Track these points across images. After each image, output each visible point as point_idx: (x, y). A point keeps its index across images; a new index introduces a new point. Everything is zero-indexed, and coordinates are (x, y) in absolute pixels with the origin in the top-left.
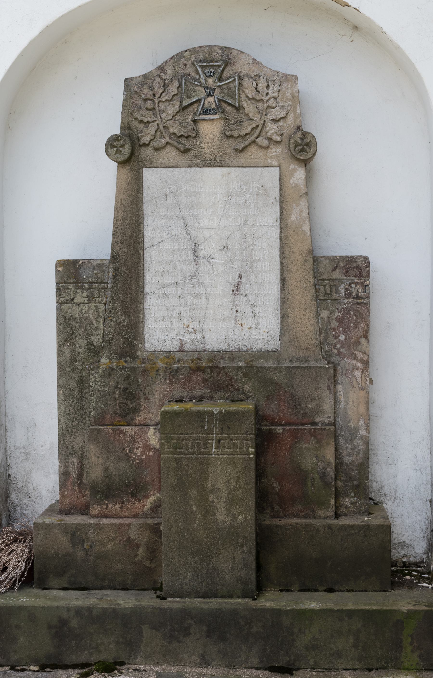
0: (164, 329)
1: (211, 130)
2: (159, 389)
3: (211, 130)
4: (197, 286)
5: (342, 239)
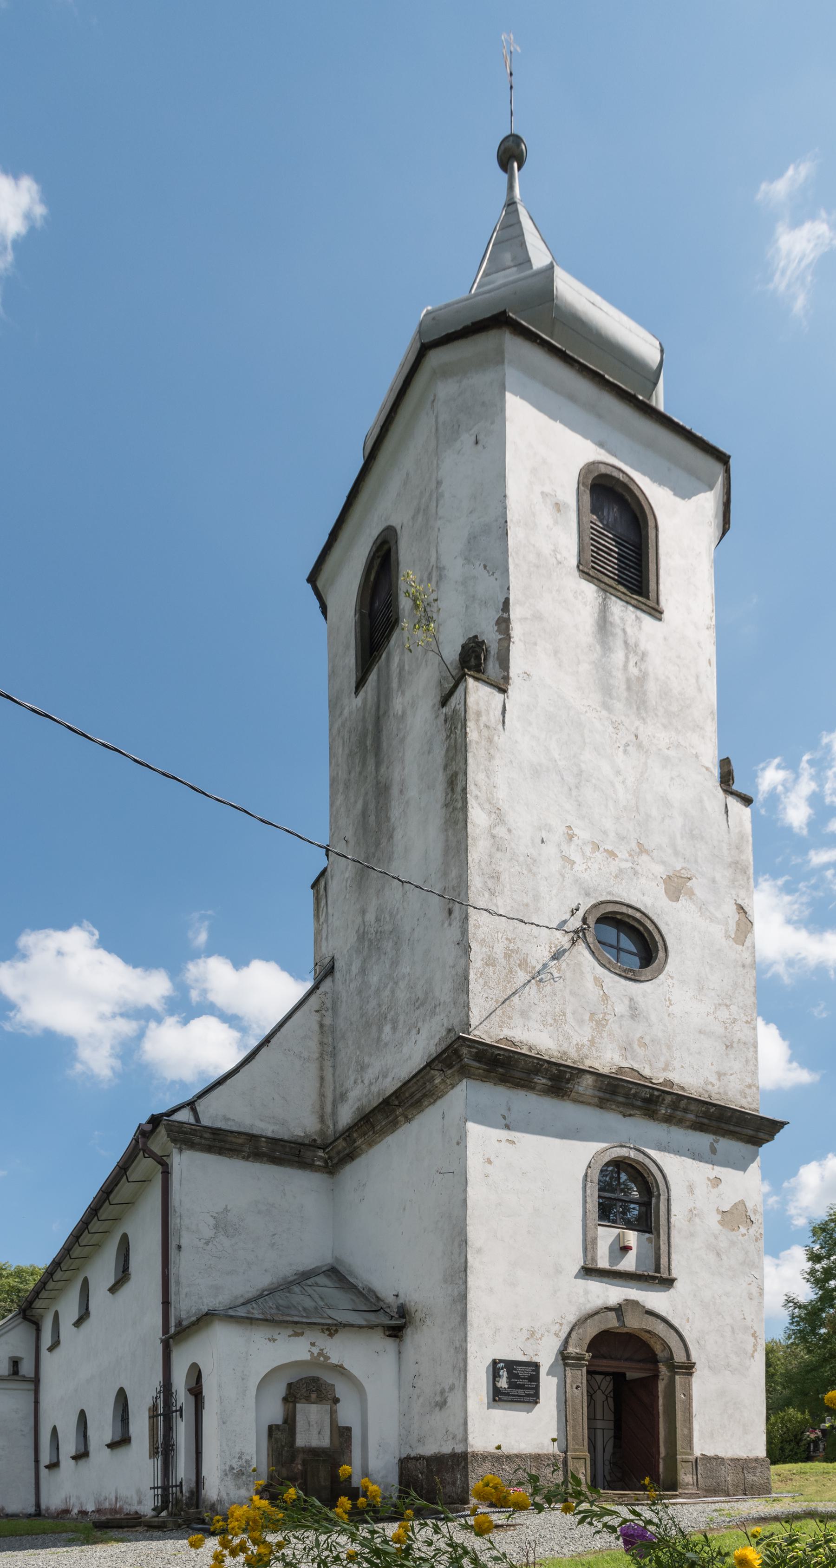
0: (301, 1441)
1: (314, 1396)
3: (314, 1396)
5: (343, 1422)
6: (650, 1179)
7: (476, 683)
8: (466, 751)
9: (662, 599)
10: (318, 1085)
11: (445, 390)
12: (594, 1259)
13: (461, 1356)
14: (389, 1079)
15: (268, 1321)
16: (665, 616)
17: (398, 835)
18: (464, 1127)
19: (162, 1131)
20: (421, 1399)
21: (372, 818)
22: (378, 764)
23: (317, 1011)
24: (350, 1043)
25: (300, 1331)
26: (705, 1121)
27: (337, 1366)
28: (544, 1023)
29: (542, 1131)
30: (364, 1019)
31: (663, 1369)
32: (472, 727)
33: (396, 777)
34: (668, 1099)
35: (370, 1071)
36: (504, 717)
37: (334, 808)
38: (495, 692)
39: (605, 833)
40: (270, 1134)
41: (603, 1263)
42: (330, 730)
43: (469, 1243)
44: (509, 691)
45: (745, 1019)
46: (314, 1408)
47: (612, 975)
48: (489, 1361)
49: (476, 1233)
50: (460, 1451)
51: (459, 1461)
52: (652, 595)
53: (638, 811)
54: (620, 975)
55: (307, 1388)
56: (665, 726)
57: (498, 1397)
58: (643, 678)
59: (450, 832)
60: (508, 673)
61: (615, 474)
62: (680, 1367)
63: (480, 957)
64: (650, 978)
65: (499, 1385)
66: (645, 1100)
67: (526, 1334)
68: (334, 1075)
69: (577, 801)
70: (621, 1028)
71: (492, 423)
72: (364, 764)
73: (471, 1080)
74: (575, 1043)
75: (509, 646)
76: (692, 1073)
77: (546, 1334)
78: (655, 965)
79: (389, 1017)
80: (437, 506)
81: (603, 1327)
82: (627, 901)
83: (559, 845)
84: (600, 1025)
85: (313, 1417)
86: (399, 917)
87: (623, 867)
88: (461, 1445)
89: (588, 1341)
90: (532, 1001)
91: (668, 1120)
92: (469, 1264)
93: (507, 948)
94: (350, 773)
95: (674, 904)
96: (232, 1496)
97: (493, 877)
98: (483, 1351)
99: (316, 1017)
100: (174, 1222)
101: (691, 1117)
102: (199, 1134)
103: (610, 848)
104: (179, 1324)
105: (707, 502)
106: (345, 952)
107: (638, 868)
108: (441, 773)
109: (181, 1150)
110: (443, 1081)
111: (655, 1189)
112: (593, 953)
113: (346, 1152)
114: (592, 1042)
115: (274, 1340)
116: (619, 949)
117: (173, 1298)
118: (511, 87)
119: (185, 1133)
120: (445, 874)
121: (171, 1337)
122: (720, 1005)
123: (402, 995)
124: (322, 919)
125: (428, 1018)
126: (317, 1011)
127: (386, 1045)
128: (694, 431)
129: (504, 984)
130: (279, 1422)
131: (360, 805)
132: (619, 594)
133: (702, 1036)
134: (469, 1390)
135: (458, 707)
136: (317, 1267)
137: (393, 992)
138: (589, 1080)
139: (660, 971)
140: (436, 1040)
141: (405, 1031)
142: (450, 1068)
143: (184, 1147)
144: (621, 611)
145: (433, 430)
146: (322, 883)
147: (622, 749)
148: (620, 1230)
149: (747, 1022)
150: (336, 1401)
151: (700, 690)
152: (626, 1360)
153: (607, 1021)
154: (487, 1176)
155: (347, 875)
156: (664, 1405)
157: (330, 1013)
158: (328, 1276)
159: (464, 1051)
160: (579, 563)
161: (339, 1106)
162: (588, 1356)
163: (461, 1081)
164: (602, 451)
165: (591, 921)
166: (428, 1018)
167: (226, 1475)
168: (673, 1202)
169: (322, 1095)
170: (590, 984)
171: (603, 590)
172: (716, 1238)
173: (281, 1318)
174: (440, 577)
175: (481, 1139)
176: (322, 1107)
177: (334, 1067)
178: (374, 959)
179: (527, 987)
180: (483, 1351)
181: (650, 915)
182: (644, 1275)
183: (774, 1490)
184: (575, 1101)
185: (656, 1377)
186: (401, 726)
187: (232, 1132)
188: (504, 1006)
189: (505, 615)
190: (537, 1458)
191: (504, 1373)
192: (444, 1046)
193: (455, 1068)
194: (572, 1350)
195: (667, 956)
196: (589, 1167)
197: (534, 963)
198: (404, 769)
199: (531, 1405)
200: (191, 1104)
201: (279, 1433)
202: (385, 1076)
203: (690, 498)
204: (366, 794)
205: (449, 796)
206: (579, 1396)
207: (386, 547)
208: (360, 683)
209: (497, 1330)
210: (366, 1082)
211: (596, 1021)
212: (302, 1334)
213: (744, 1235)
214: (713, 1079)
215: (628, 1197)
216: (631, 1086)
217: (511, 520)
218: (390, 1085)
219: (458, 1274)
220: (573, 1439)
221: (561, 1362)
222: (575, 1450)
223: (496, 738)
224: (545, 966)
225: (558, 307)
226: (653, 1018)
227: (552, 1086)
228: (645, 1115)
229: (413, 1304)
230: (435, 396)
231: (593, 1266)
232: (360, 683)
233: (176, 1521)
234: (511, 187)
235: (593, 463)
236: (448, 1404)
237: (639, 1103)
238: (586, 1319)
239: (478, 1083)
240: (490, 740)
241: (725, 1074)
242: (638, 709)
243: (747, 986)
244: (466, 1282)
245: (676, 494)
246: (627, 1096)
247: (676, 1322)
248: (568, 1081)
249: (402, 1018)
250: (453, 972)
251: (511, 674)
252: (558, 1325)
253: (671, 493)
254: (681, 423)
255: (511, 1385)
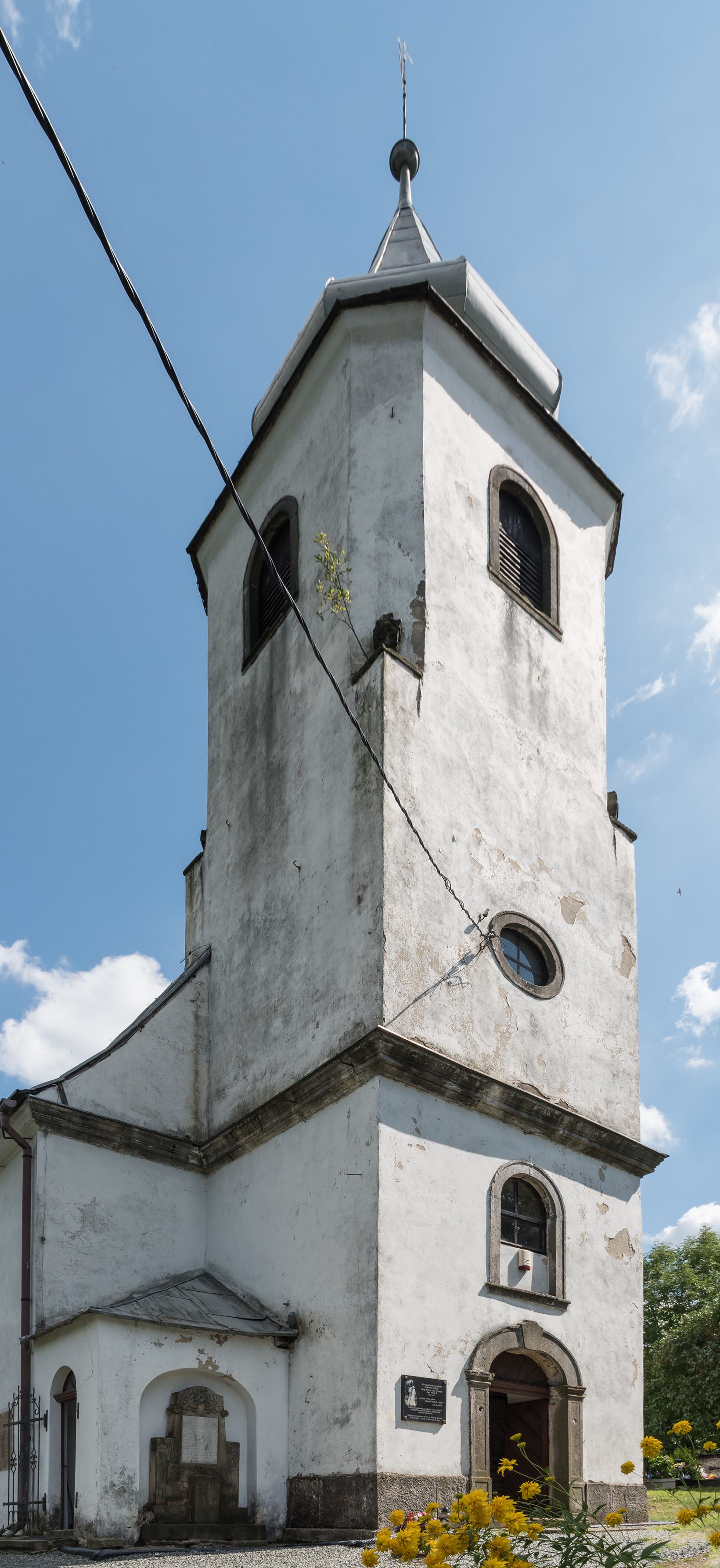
0: (187, 1457)
1: (201, 1407)
2: (187, 1473)
3: (201, 1407)
4: (566, 1536)
5: (231, 1437)
6: (546, 1200)
7: (393, 662)
8: (383, 730)
9: (562, 620)
10: (192, 1079)
11: (359, 355)
12: (497, 1277)
13: (369, 1371)
14: (278, 1076)
15: (156, 1324)
16: (565, 637)
17: (294, 819)
18: (376, 1127)
19: (26, 1109)
20: (317, 1416)
21: (261, 802)
22: (270, 745)
23: (192, 1001)
24: (230, 1037)
25: (187, 1336)
26: (597, 1146)
27: (226, 1376)
28: (453, 1027)
29: (449, 1141)
30: (248, 1012)
31: (554, 1393)
32: (389, 707)
33: (293, 757)
34: (567, 1119)
35: (255, 1066)
36: (419, 703)
37: (213, 791)
38: (410, 675)
39: (509, 842)
40: (141, 1125)
41: (504, 1282)
42: (209, 709)
43: (380, 1250)
44: (424, 677)
45: (628, 1050)
46: (201, 1421)
47: (515, 988)
48: (397, 1378)
49: (387, 1240)
50: (366, 1472)
51: (368, 1483)
52: (553, 613)
53: (539, 827)
54: (522, 989)
55: (191, 1399)
56: (563, 747)
57: (406, 1415)
58: (544, 694)
59: (361, 816)
60: (423, 658)
61: (522, 483)
62: (573, 1392)
63: (394, 949)
64: (548, 996)
65: (408, 1403)
66: (546, 1119)
67: (433, 1351)
68: (209, 1070)
69: (485, 805)
70: (522, 1043)
71: (409, 398)
72: (252, 743)
73: (384, 1078)
74: (481, 1052)
75: (424, 631)
76: (584, 1096)
77: (452, 1351)
78: (553, 984)
79: (280, 1010)
80: (349, 475)
81: (505, 1347)
82: (530, 916)
83: (468, 847)
84: (504, 1037)
85: (200, 1431)
86: (294, 904)
87: (525, 880)
88: (369, 1466)
89: (491, 1360)
90: (442, 1003)
91: (564, 1141)
92: (380, 1273)
93: (420, 944)
94: (234, 754)
95: (570, 926)
96: (113, 1515)
97: (407, 867)
98: (394, 1364)
99: (191, 1007)
100: (37, 1211)
101: (585, 1140)
102: (67, 1117)
103: (514, 859)
104: (41, 1324)
105: (600, 534)
106: (225, 941)
107: (538, 883)
108: (350, 754)
109: (46, 1133)
110: (352, 1077)
111: (551, 1211)
112: (498, 962)
113: (226, 1151)
114: (497, 1053)
115: (161, 1345)
116: (519, 964)
117: (34, 1295)
118: (404, 95)
119: (53, 1115)
120: (354, 860)
121: (34, 1338)
122: (608, 1033)
123: (297, 987)
124: (196, 906)
125: (329, 1011)
126: (192, 1001)
127: (276, 1039)
128: (593, 459)
129: (417, 981)
130: (163, 1435)
131: (246, 787)
132: (524, 605)
133: (593, 1062)
134: (378, 1407)
135: (372, 684)
136: (189, 1272)
137: (285, 983)
138: (496, 1091)
139: (558, 990)
140: (341, 1034)
141: (300, 1025)
142: (361, 1064)
143: (49, 1130)
144: (526, 623)
145: (345, 396)
146: (197, 869)
147: (525, 761)
148: (518, 1249)
149: (630, 1053)
150: (224, 1414)
151: (593, 719)
152: (521, 1382)
153: (510, 1034)
154: (398, 1181)
155: (229, 861)
156: (555, 1430)
157: (205, 1005)
158: (204, 1282)
159: (381, 1045)
160: (489, 564)
161: (215, 1103)
162: (491, 1376)
163: (372, 1077)
164: (510, 458)
165: (497, 930)
166: (329, 1011)
167: (107, 1492)
168: (567, 1225)
169: (196, 1090)
170: (495, 994)
171: (510, 597)
172: (603, 1264)
173: (168, 1321)
174: (351, 550)
175: (393, 1143)
176: (196, 1103)
177: (209, 1062)
178: (262, 949)
179: (438, 988)
180: (394, 1364)
181: (549, 933)
182: (542, 1297)
183: (650, 1518)
184: (481, 1112)
185: (545, 1401)
186: (300, 705)
187: (103, 1118)
188: (416, 1003)
189: (421, 599)
190: (443, 1482)
191: (413, 1391)
192: (349, 1042)
193: (365, 1065)
194: (477, 1369)
195: (563, 977)
196: (493, 1181)
197: (445, 964)
198: (303, 749)
199: (437, 1425)
200: (58, 1084)
201: (164, 1447)
202: (274, 1072)
203: (585, 528)
204: (255, 776)
205: (360, 778)
206: (482, 1418)
207: (282, 519)
208: (248, 660)
209: (406, 1345)
210: (250, 1078)
211: (501, 1033)
212: (190, 1340)
213: (627, 1263)
214: (602, 1106)
215: (526, 1215)
216: (534, 1102)
217: (428, 502)
218: (280, 1083)
219: (366, 1283)
220: (477, 1463)
221: (466, 1381)
222: (478, 1474)
223: (411, 723)
224: (454, 969)
225: (469, 303)
226: (551, 1037)
227: (461, 1094)
228: (544, 1134)
229: (307, 1313)
230: (347, 361)
231: (496, 1284)
232: (248, 660)
233: (46, 1542)
234: (404, 193)
235: (503, 467)
236: (351, 1422)
237: (540, 1121)
238: (490, 1338)
239: (391, 1082)
240: (406, 725)
241: (612, 1102)
242: (540, 724)
243: (630, 1018)
244: (376, 1292)
245: (573, 521)
246: (530, 1112)
247: (569, 1346)
248: (477, 1090)
249: (296, 1011)
250: (363, 963)
251: (426, 661)
252: (463, 1343)
253: (569, 519)
254: (583, 449)
255: (420, 1403)
